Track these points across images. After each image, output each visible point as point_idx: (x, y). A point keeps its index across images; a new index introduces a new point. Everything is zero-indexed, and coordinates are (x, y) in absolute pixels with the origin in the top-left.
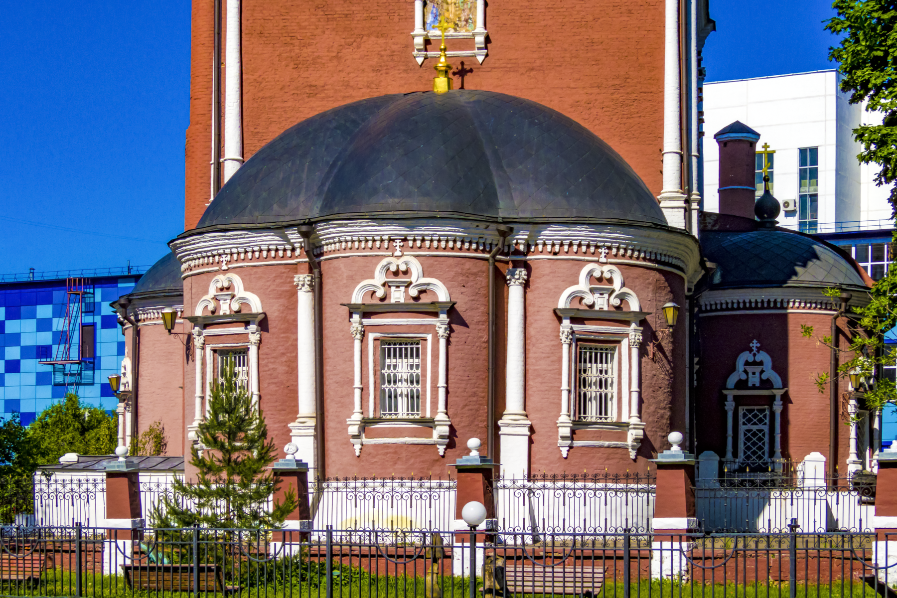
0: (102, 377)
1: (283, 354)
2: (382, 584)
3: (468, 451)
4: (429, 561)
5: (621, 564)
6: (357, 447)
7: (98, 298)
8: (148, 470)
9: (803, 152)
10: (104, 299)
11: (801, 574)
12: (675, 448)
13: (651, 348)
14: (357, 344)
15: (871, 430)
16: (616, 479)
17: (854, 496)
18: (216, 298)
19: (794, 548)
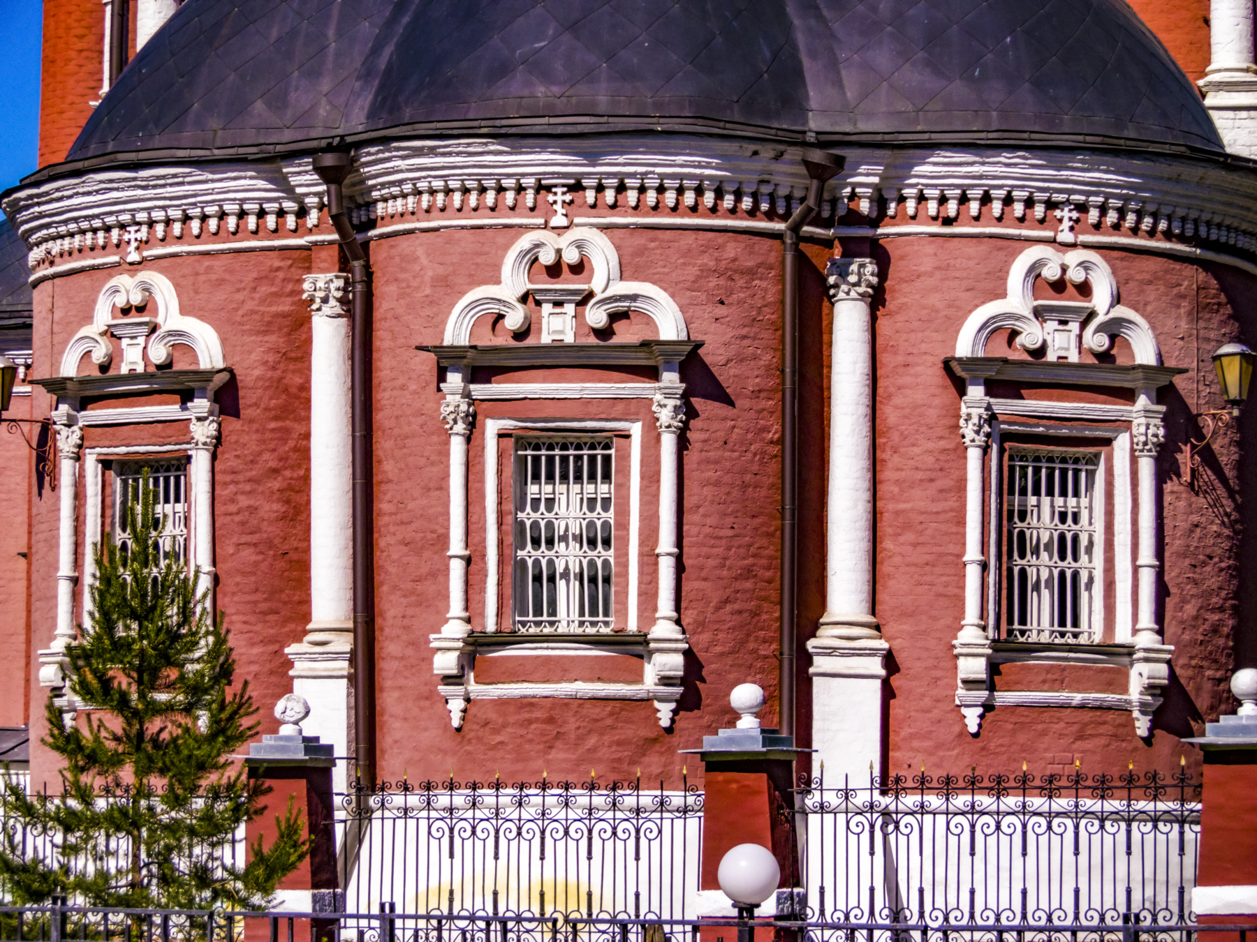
1: (275, 471)
3: (732, 716)
6: (456, 706)
13: (1185, 458)
14: (457, 447)
18: (111, 334)
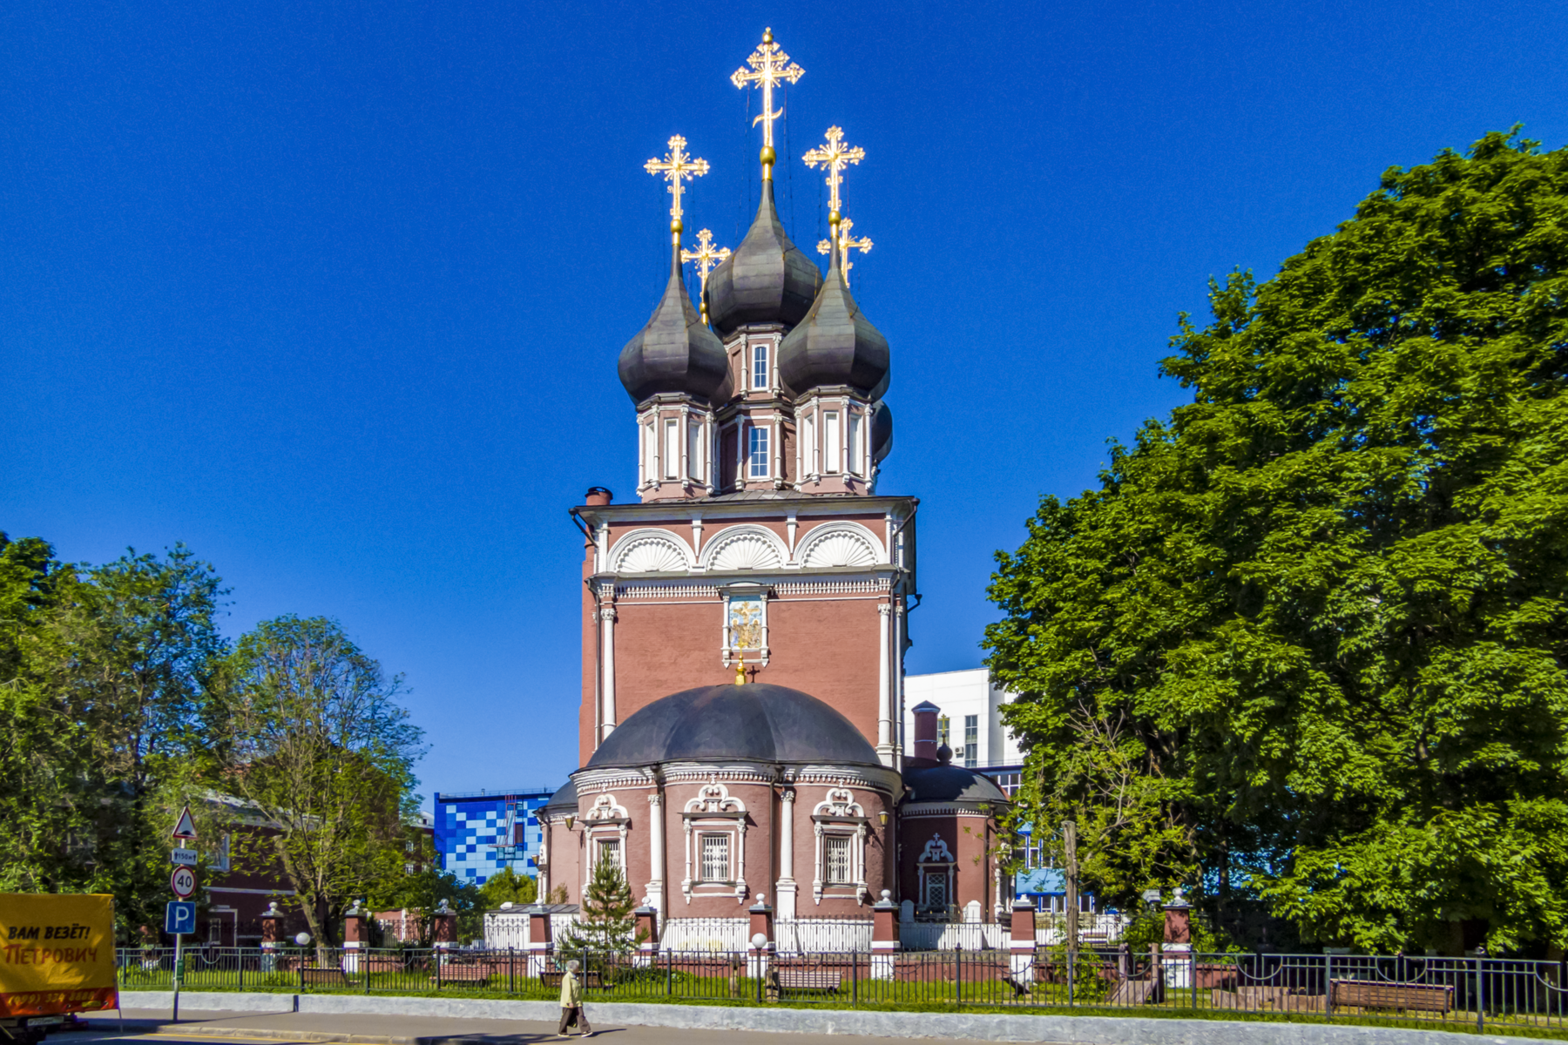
0: (528, 855)
2: (702, 982)
3: (757, 901)
4: (732, 968)
5: (851, 969)
6: (688, 899)
7: (525, 807)
8: (557, 912)
9: (968, 718)
10: (529, 808)
11: (963, 975)
12: (886, 900)
13: (871, 839)
14: (688, 837)
15: (1010, 887)
16: (849, 918)
17: (999, 926)
18: (599, 809)
19: (959, 962)
